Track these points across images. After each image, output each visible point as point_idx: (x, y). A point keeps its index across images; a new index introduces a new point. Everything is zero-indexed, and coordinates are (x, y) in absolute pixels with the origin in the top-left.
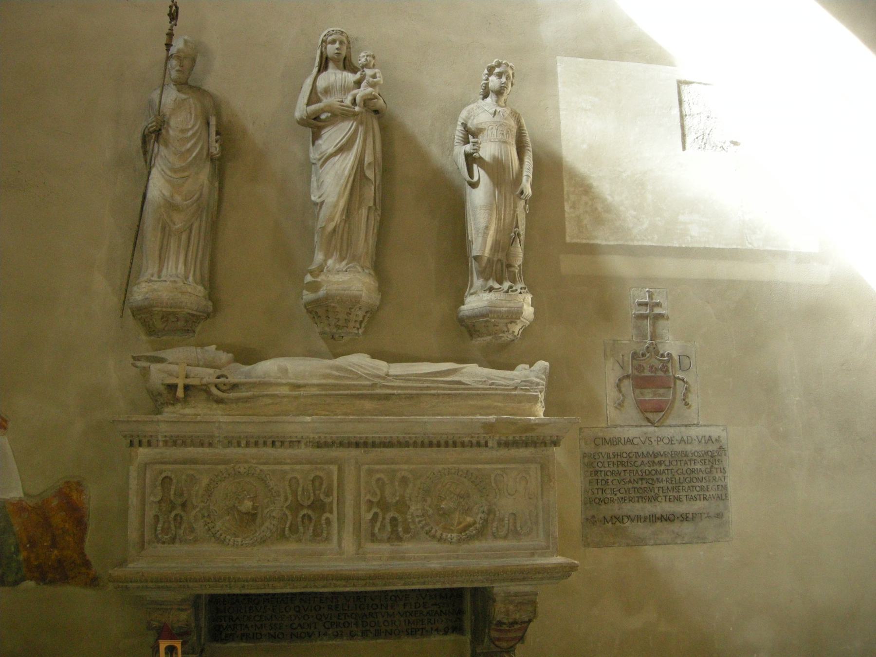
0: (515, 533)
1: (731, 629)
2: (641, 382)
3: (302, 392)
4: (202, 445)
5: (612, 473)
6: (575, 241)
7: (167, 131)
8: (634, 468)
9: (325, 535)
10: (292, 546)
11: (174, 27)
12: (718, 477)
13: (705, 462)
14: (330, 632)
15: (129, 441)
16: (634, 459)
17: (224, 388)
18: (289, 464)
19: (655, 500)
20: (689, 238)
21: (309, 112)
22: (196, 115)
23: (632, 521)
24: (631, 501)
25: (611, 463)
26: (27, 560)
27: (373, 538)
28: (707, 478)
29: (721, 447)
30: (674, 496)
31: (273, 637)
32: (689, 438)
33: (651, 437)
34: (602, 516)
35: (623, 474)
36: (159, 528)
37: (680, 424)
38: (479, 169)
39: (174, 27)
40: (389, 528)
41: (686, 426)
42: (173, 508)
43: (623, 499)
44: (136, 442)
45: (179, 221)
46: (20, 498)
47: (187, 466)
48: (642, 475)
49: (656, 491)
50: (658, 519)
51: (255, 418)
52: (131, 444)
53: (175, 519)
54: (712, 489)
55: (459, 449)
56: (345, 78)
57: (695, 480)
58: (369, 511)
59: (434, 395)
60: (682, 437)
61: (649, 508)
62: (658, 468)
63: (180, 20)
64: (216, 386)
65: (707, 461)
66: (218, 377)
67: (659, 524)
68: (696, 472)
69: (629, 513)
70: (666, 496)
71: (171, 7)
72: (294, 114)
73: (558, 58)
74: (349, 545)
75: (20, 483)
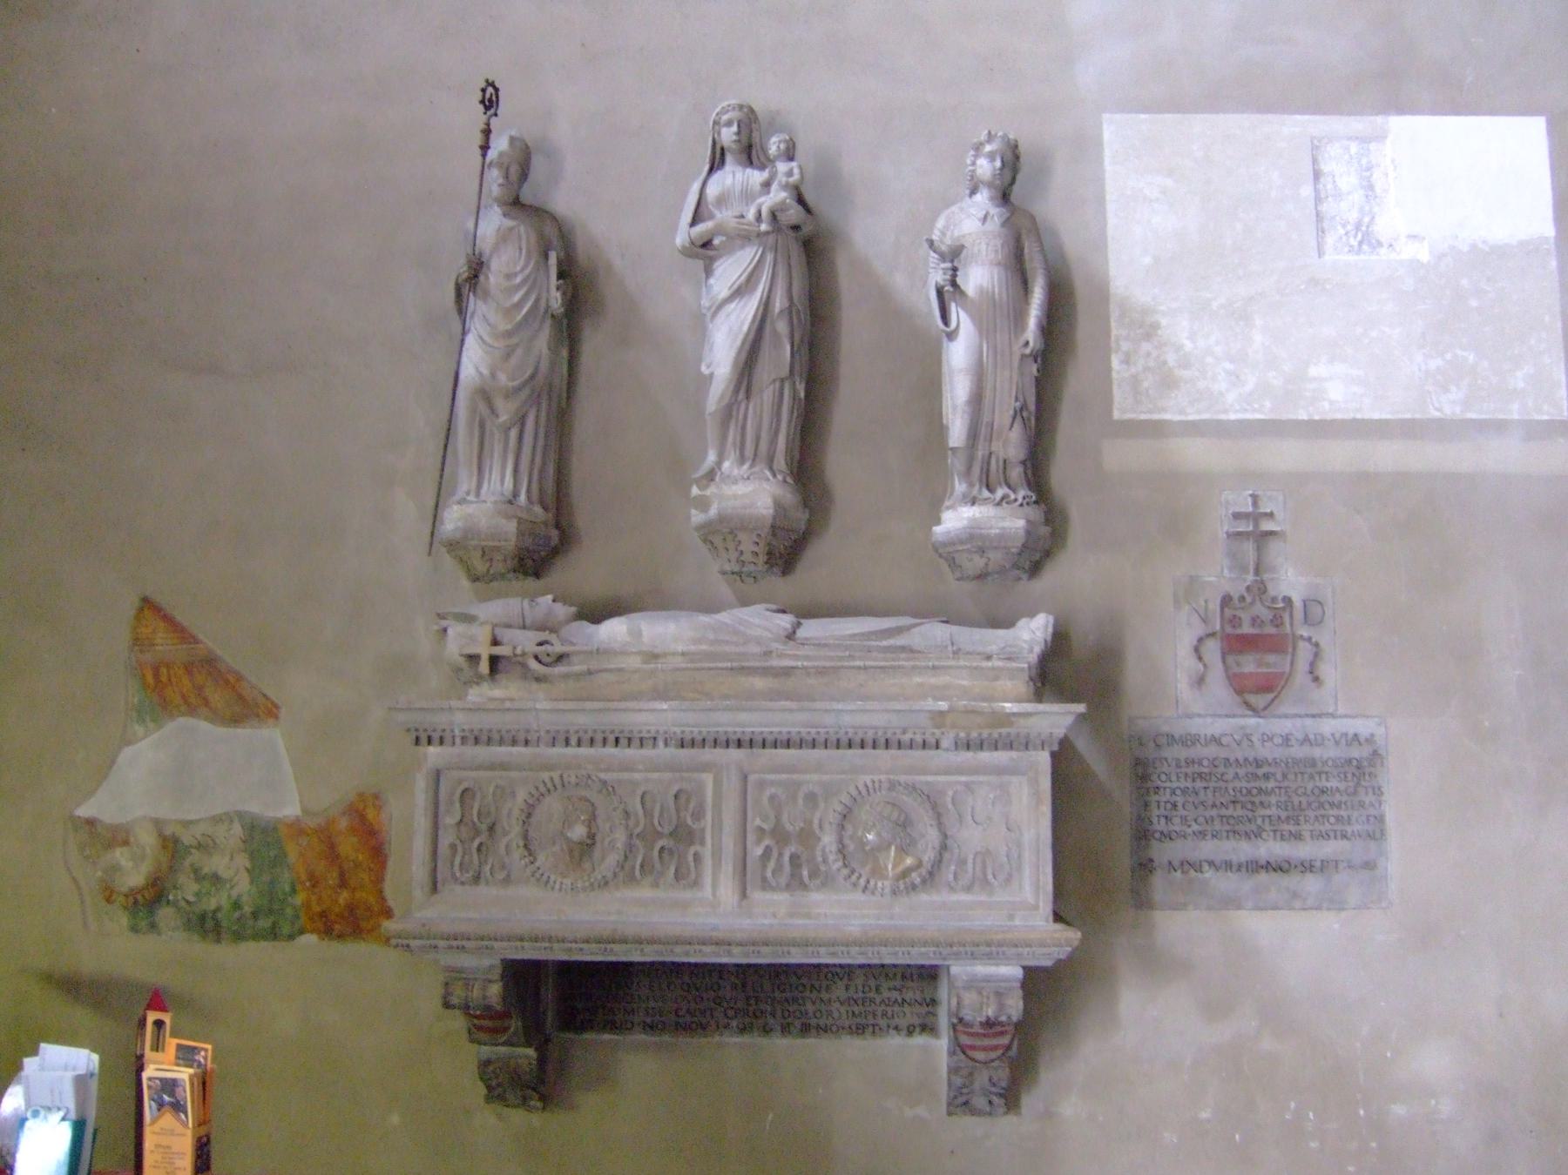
0: (982, 882)
1: (1389, 1055)
2: (1237, 644)
3: (660, 666)
4: (514, 742)
5: (1185, 791)
6: (1128, 416)
7: (487, 278)
8: (1222, 784)
9: (693, 876)
10: (645, 892)
11: (494, 121)
12: (1367, 802)
13: (1346, 777)
14: (734, 1023)
15: (414, 737)
16: (1221, 769)
17: (548, 660)
18: (641, 771)
19: (1256, 836)
20: (1326, 405)
21: (692, 236)
22: (529, 252)
23: (1217, 868)
24: (1216, 836)
25: (1182, 775)
26: (307, 905)
27: (765, 885)
28: (1349, 804)
29: (1375, 753)
30: (1290, 831)
31: (650, 1028)
32: (1318, 737)
33: (1251, 734)
34: (1165, 861)
35: (1202, 793)
36: (457, 862)
37: (1303, 713)
38: (960, 310)
39: (494, 121)
40: (787, 868)
41: (1313, 716)
42: (477, 833)
43: (1202, 834)
44: (424, 739)
45: (506, 411)
46: (297, 817)
47: (497, 773)
48: (1235, 796)
49: (1259, 821)
50: (1262, 867)
51: (588, 705)
52: (417, 741)
53: (479, 850)
54: (1357, 821)
55: (893, 752)
56: (748, 178)
57: (1327, 806)
58: (759, 841)
59: (859, 668)
60: (1307, 735)
61: (1244, 850)
62: (1264, 785)
63: (504, 107)
64: (536, 657)
65: (1349, 776)
66: (540, 644)
67: (1263, 877)
68: (1329, 793)
69: (1211, 857)
70: (1275, 831)
71: (484, 91)
72: (674, 239)
73: (1106, 116)
74: (727, 892)
75: (297, 795)
